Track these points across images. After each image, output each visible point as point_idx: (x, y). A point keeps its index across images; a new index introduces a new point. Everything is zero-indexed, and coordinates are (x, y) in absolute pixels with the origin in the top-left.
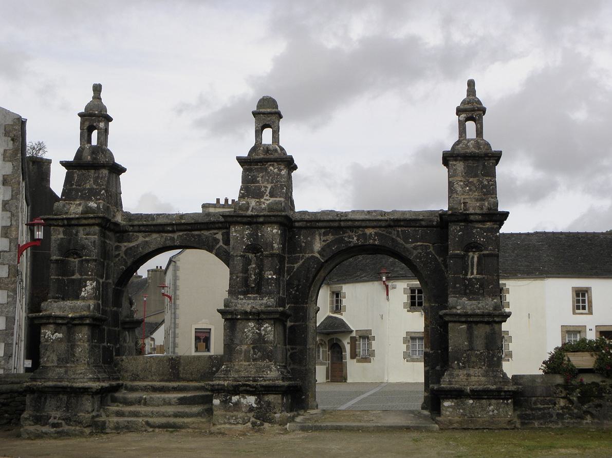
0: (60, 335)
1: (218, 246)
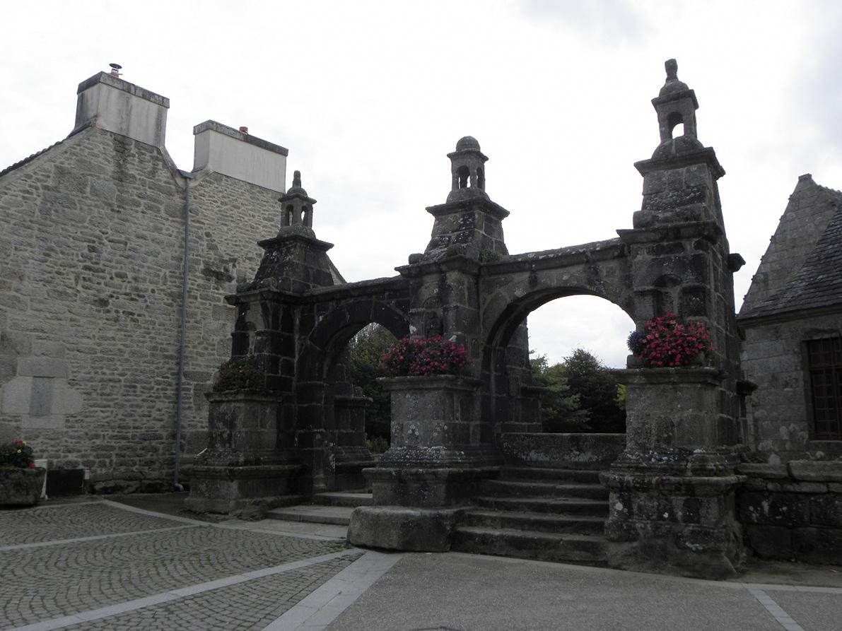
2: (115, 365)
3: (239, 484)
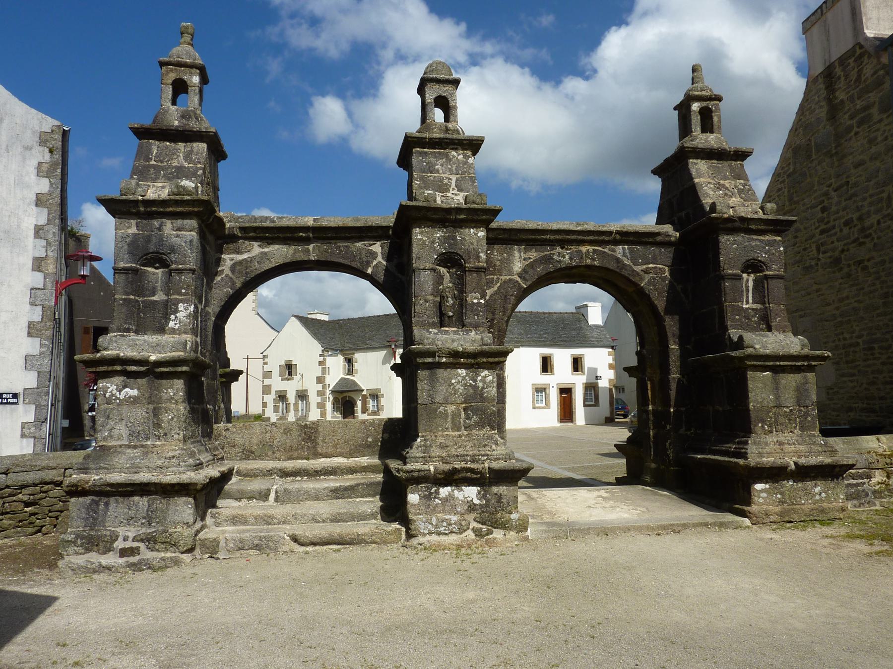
0: (134, 392)
1: (375, 263)
2: (852, 327)
3: (380, 482)
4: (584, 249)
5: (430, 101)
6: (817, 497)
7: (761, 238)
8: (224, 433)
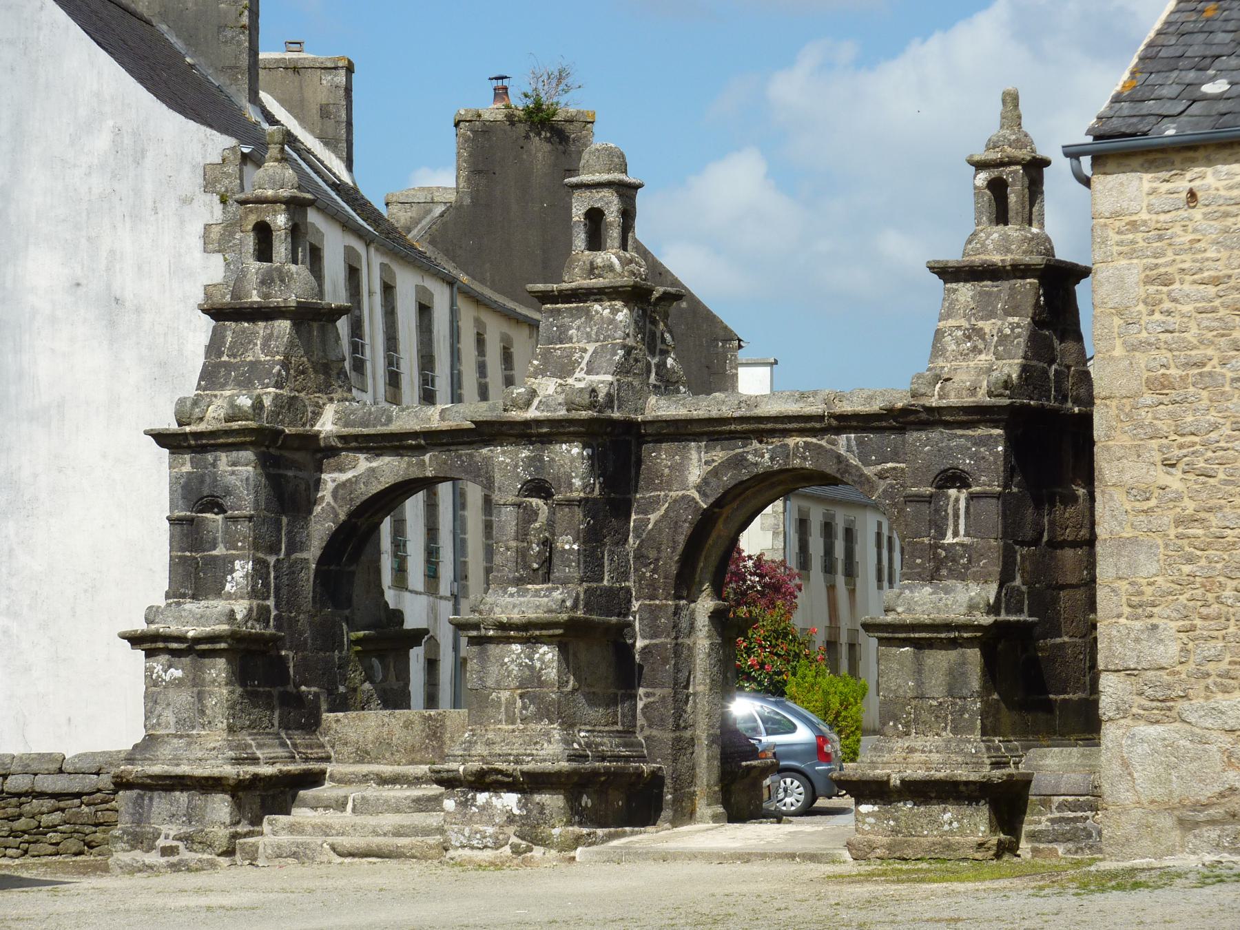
4: (792, 441)
5: (577, 218)
6: (946, 827)
7: (970, 432)
8: (334, 725)
